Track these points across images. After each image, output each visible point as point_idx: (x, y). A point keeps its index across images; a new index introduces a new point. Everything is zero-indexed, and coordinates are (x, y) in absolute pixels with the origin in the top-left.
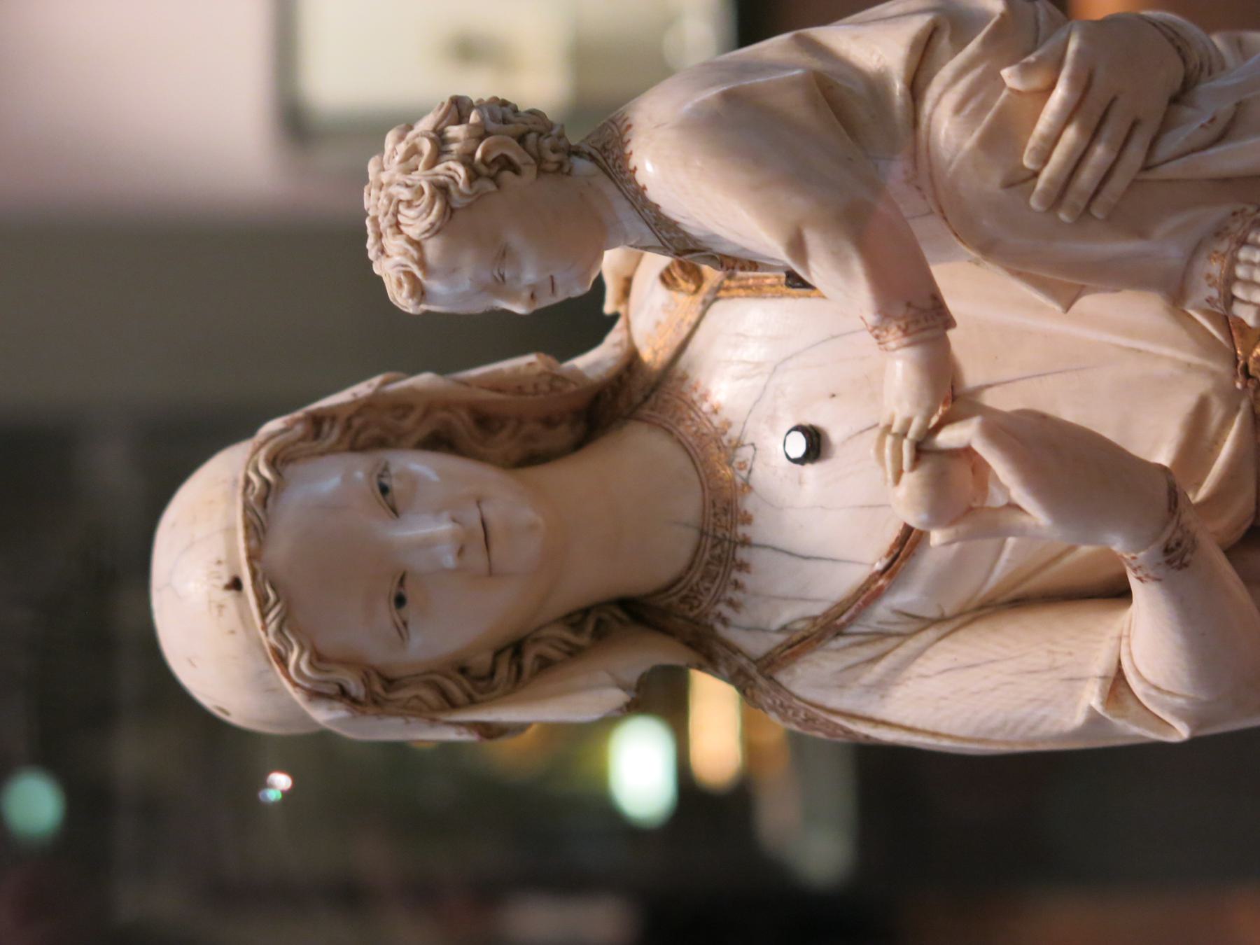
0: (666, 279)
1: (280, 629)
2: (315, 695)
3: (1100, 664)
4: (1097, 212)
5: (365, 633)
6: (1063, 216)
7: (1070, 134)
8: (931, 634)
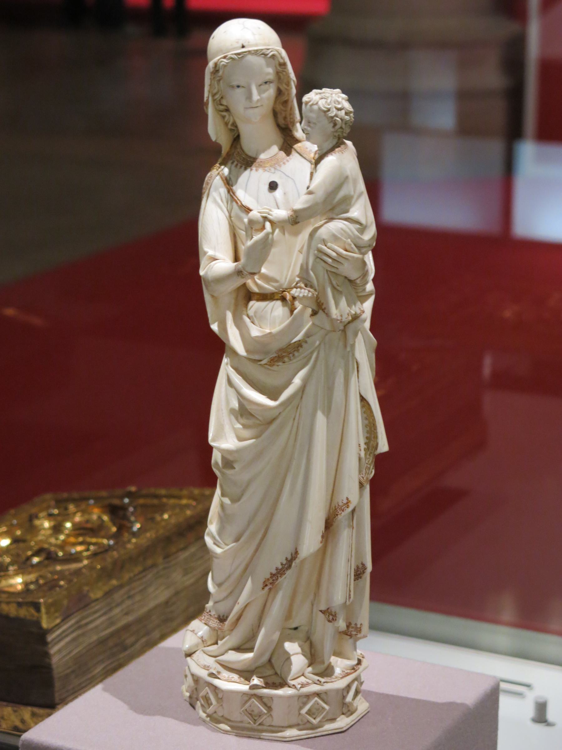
1: (231, 58)
2: (216, 64)
3: (218, 255)
6: (316, 252)
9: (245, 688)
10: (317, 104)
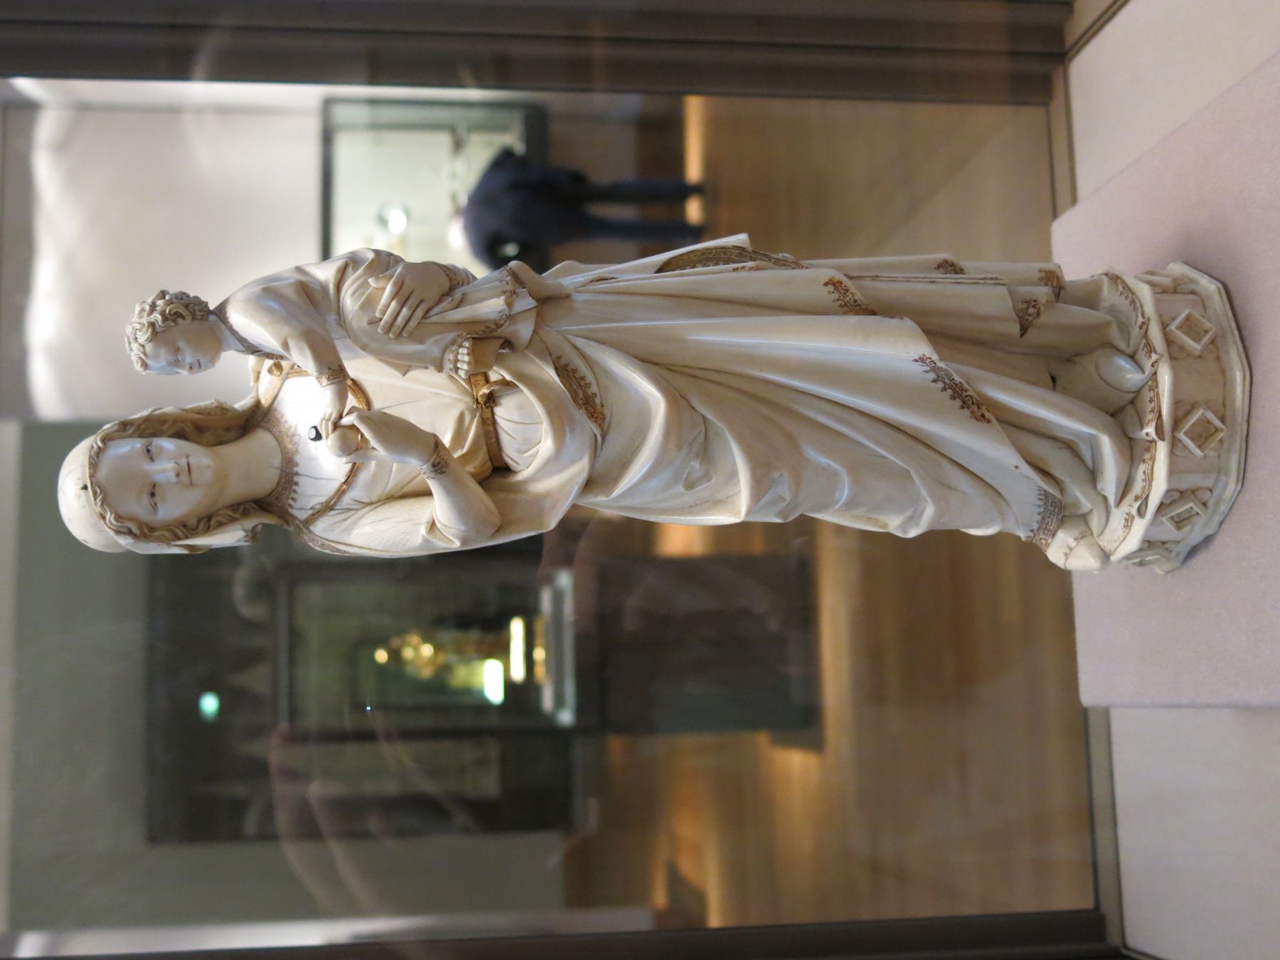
0: (270, 371)
2: (118, 532)
3: (425, 518)
4: (404, 334)
5: (138, 507)
7: (394, 304)
8: (367, 509)
9: (1162, 449)
10: (143, 346)
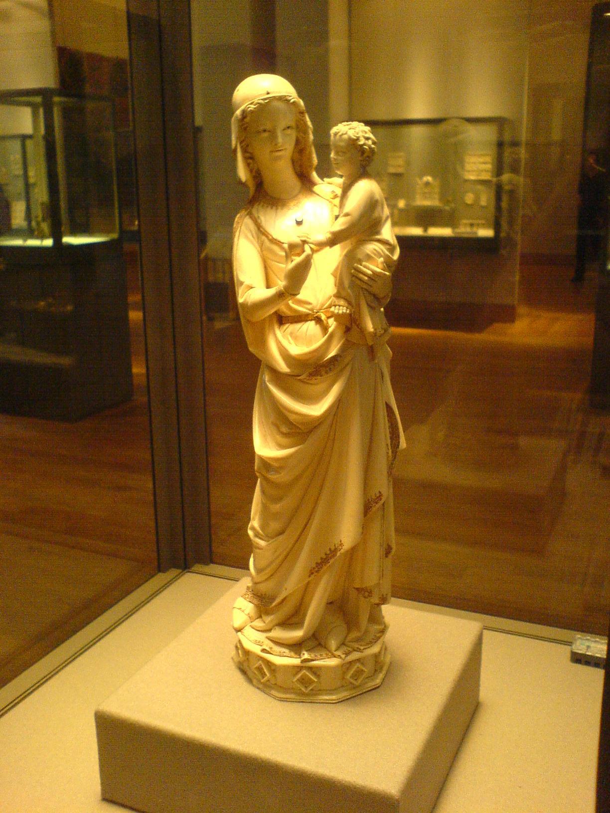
2: (244, 111)
7: (369, 272)
9: (296, 661)
